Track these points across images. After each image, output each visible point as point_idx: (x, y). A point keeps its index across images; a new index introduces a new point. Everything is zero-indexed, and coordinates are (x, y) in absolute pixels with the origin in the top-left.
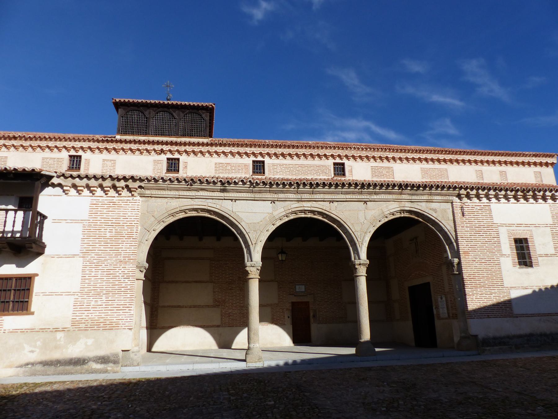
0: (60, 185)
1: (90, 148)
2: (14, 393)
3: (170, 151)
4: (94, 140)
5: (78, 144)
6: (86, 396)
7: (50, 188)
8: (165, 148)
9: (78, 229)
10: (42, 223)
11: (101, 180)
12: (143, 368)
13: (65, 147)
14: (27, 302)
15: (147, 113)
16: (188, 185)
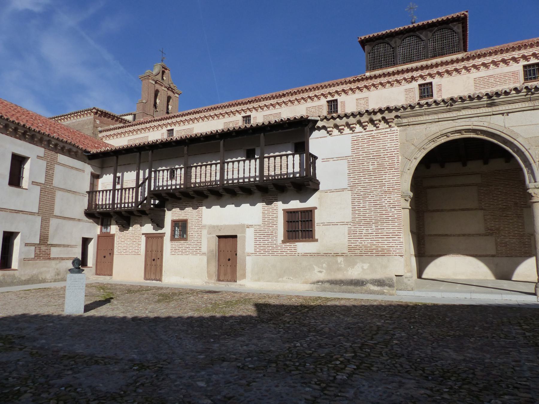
0: (324, 128)
1: (344, 91)
2: (312, 304)
3: (422, 77)
4: (346, 83)
5: (333, 90)
6: (370, 313)
7: (316, 131)
8: (415, 74)
9: (344, 166)
10: (314, 163)
11: (358, 116)
12: (417, 293)
13: (322, 94)
14: (312, 231)
15: (392, 43)
16: (447, 106)
